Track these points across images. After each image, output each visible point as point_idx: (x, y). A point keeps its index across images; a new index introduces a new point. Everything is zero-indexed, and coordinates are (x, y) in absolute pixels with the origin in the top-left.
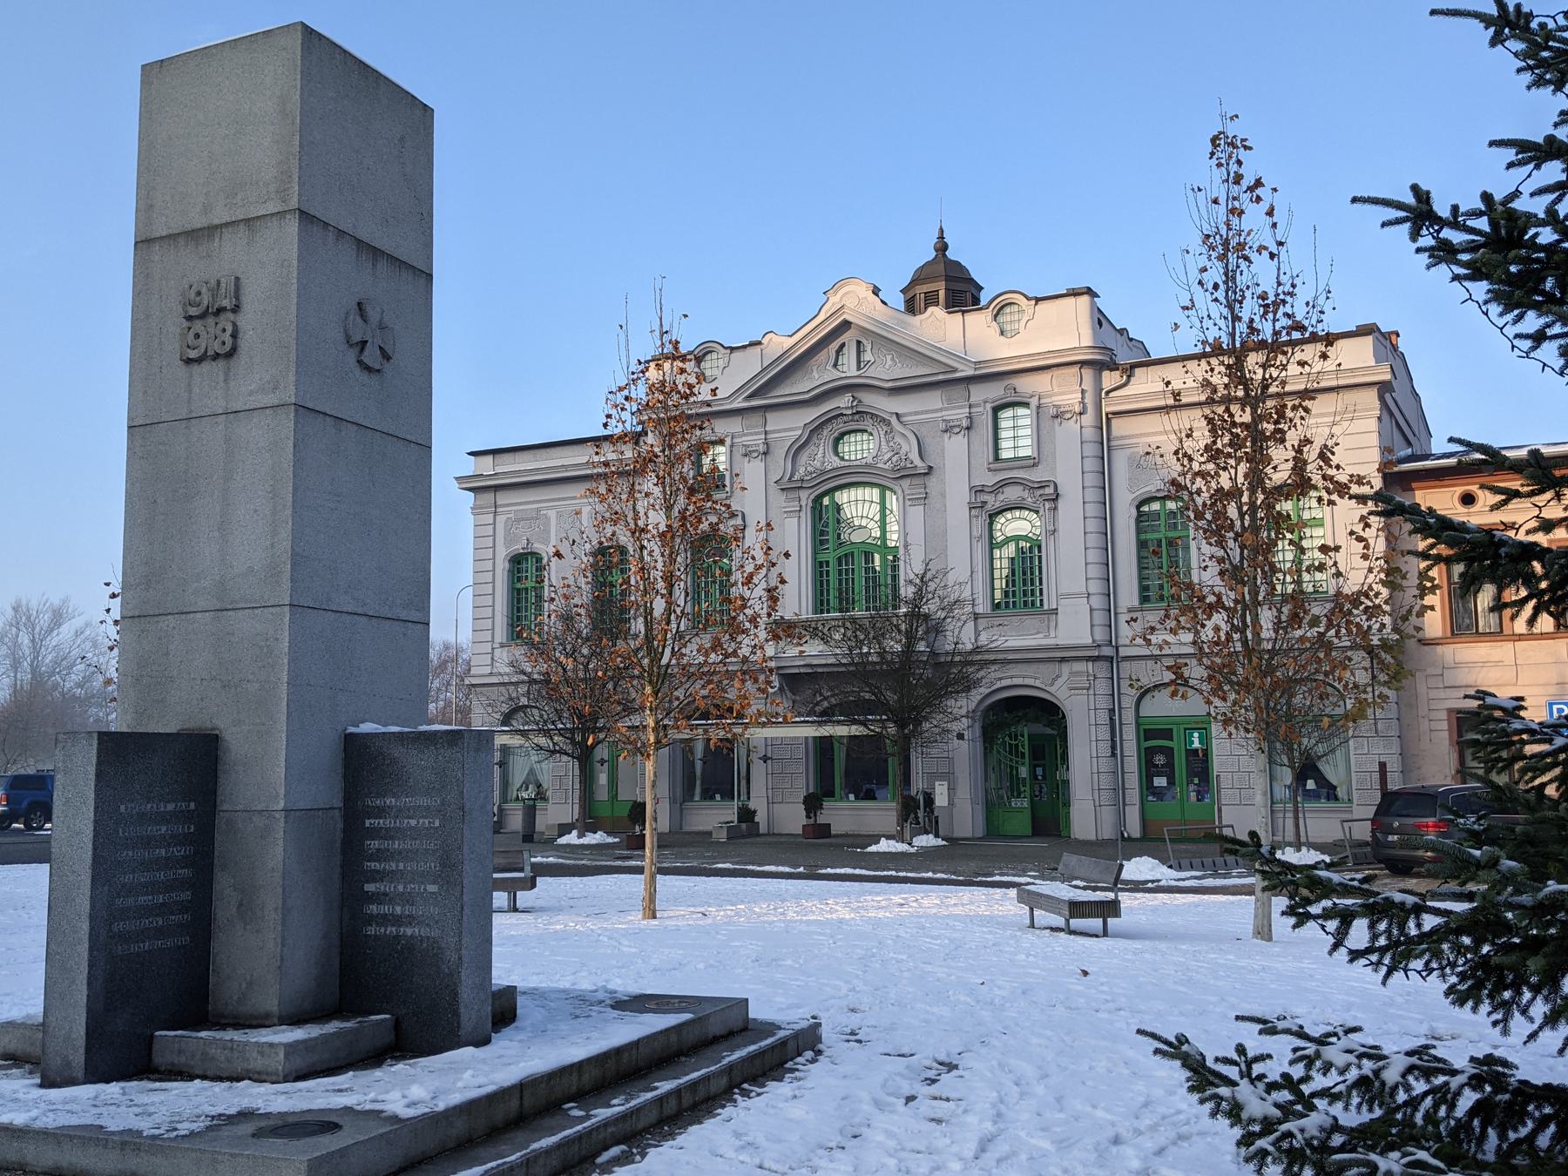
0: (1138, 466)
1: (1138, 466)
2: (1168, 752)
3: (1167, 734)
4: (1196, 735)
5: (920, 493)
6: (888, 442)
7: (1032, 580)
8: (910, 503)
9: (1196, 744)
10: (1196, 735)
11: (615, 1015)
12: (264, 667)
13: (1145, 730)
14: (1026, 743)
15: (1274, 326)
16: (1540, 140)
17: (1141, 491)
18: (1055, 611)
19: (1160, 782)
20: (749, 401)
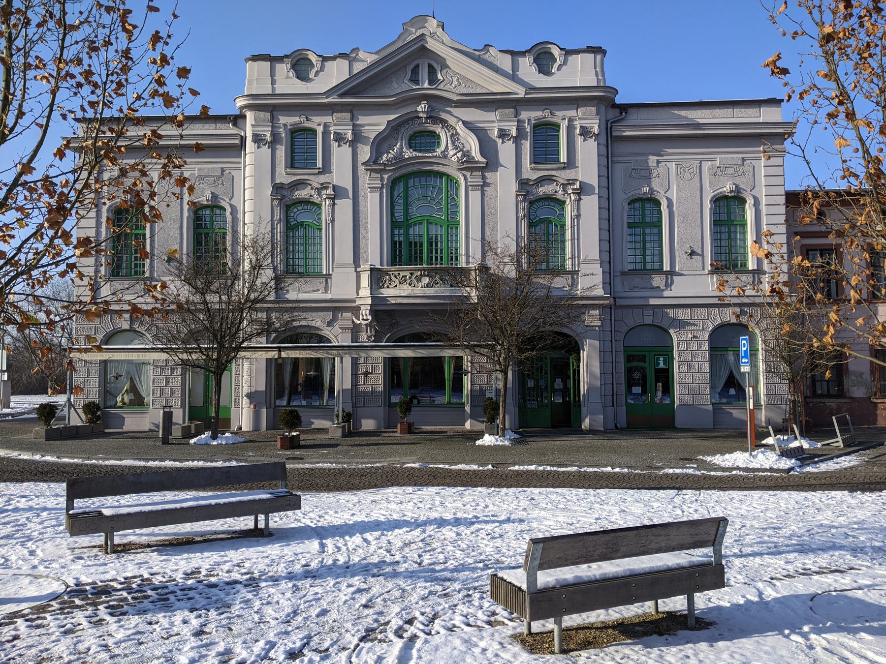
0: (630, 176)
1: (630, 176)
2: (643, 370)
3: (643, 359)
4: (661, 359)
5: (478, 182)
6: (453, 143)
7: (436, 258)
8: (470, 188)
9: (662, 365)
10: (661, 359)
11: (221, 523)
12: (120, 85)
13: (645, 355)
14: (549, 363)
15: (606, 116)
16: (351, 148)
17: (632, 193)
18: (328, 276)
19: (637, 390)
20: (341, 98)
